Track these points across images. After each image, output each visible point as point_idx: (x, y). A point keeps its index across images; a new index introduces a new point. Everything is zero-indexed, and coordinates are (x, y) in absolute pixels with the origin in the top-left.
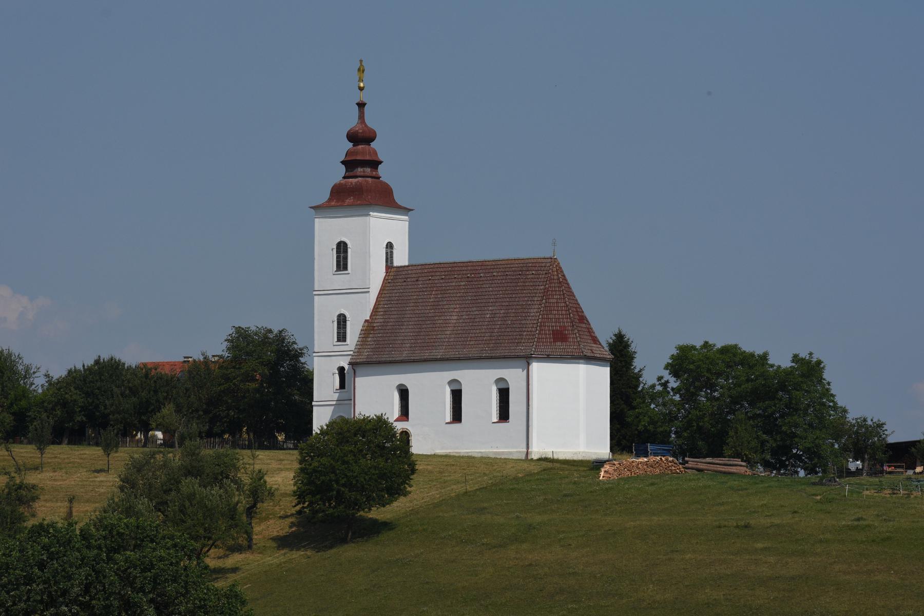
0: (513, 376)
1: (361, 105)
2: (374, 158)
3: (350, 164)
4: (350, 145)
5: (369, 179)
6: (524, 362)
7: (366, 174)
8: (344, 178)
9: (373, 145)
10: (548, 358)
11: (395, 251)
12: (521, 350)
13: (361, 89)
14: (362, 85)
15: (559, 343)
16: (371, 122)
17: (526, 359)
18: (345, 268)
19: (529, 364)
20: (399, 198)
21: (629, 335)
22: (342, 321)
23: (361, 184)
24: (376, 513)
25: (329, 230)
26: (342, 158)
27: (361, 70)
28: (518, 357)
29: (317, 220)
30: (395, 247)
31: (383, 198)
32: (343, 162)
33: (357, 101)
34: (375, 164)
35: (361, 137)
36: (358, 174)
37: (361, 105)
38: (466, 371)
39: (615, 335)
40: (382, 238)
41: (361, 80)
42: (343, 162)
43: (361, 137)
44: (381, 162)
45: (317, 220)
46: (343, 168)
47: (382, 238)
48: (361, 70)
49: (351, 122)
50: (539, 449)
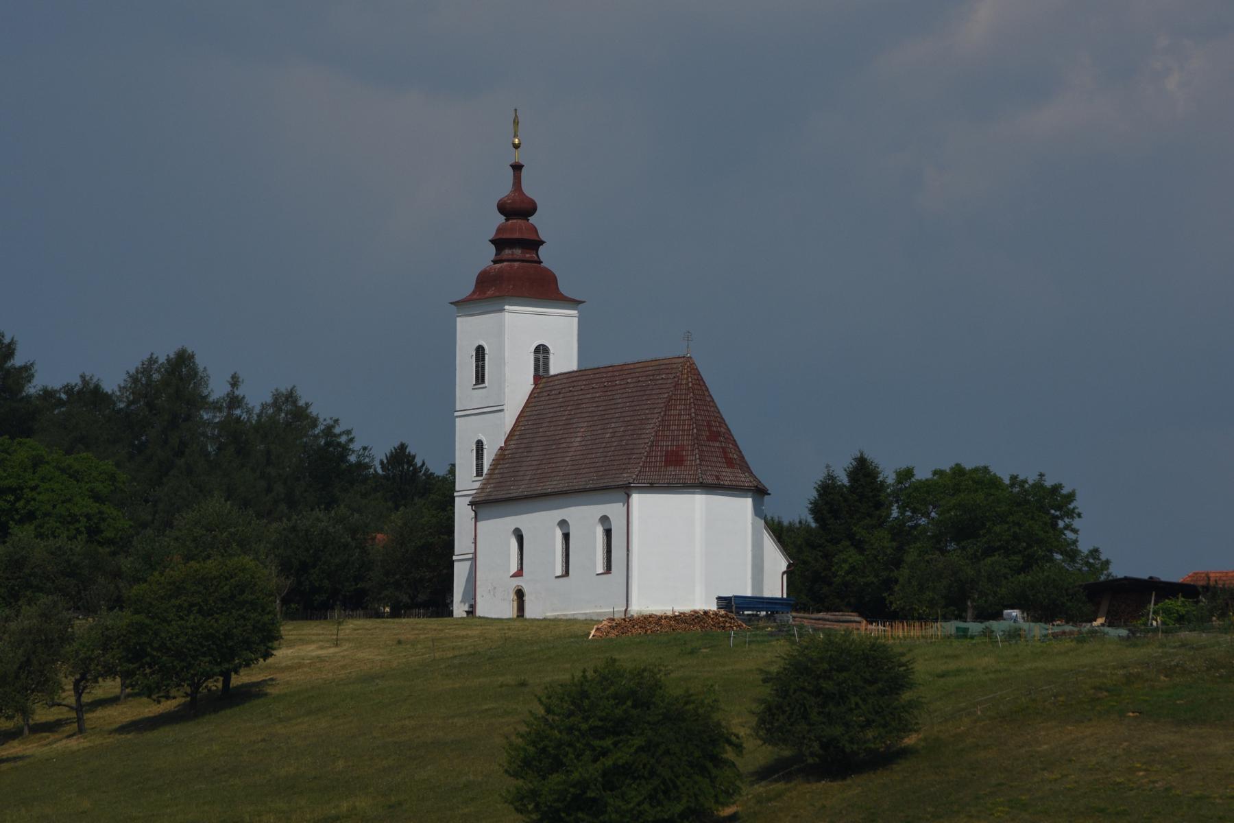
0: (614, 510)
1: (517, 168)
2: (533, 237)
3: (500, 243)
4: (502, 219)
5: (516, 264)
6: (623, 495)
7: (515, 257)
8: (495, 262)
9: (532, 220)
10: (652, 487)
11: (551, 357)
12: (625, 478)
13: (516, 147)
14: (517, 141)
15: (671, 468)
16: (529, 190)
17: (625, 491)
18: (483, 382)
19: (629, 496)
20: (564, 288)
21: (869, 455)
22: (480, 445)
23: (518, 268)
24: (240, 679)
25: (471, 330)
26: (492, 235)
27: (516, 122)
28: (618, 487)
29: (458, 319)
30: (552, 351)
31: (542, 289)
32: (492, 241)
33: (512, 162)
34: (535, 244)
35: (517, 209)
36: (505, 257)
37: (517, 168)
38: (573, 509)
39: (855, 459)
40: (528, 341)
41: (516, 136)
42: (492, 241)
43: (517, 209)
44: (542, 243)
45: (458, 319)
46: (492, 248)
47: (528, 341)
48: (516, 122)
49: (504, 189)
50: (641, 605)
